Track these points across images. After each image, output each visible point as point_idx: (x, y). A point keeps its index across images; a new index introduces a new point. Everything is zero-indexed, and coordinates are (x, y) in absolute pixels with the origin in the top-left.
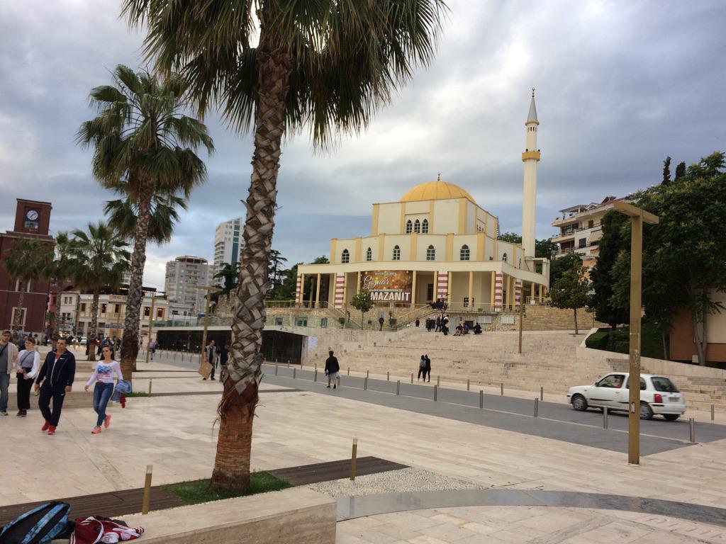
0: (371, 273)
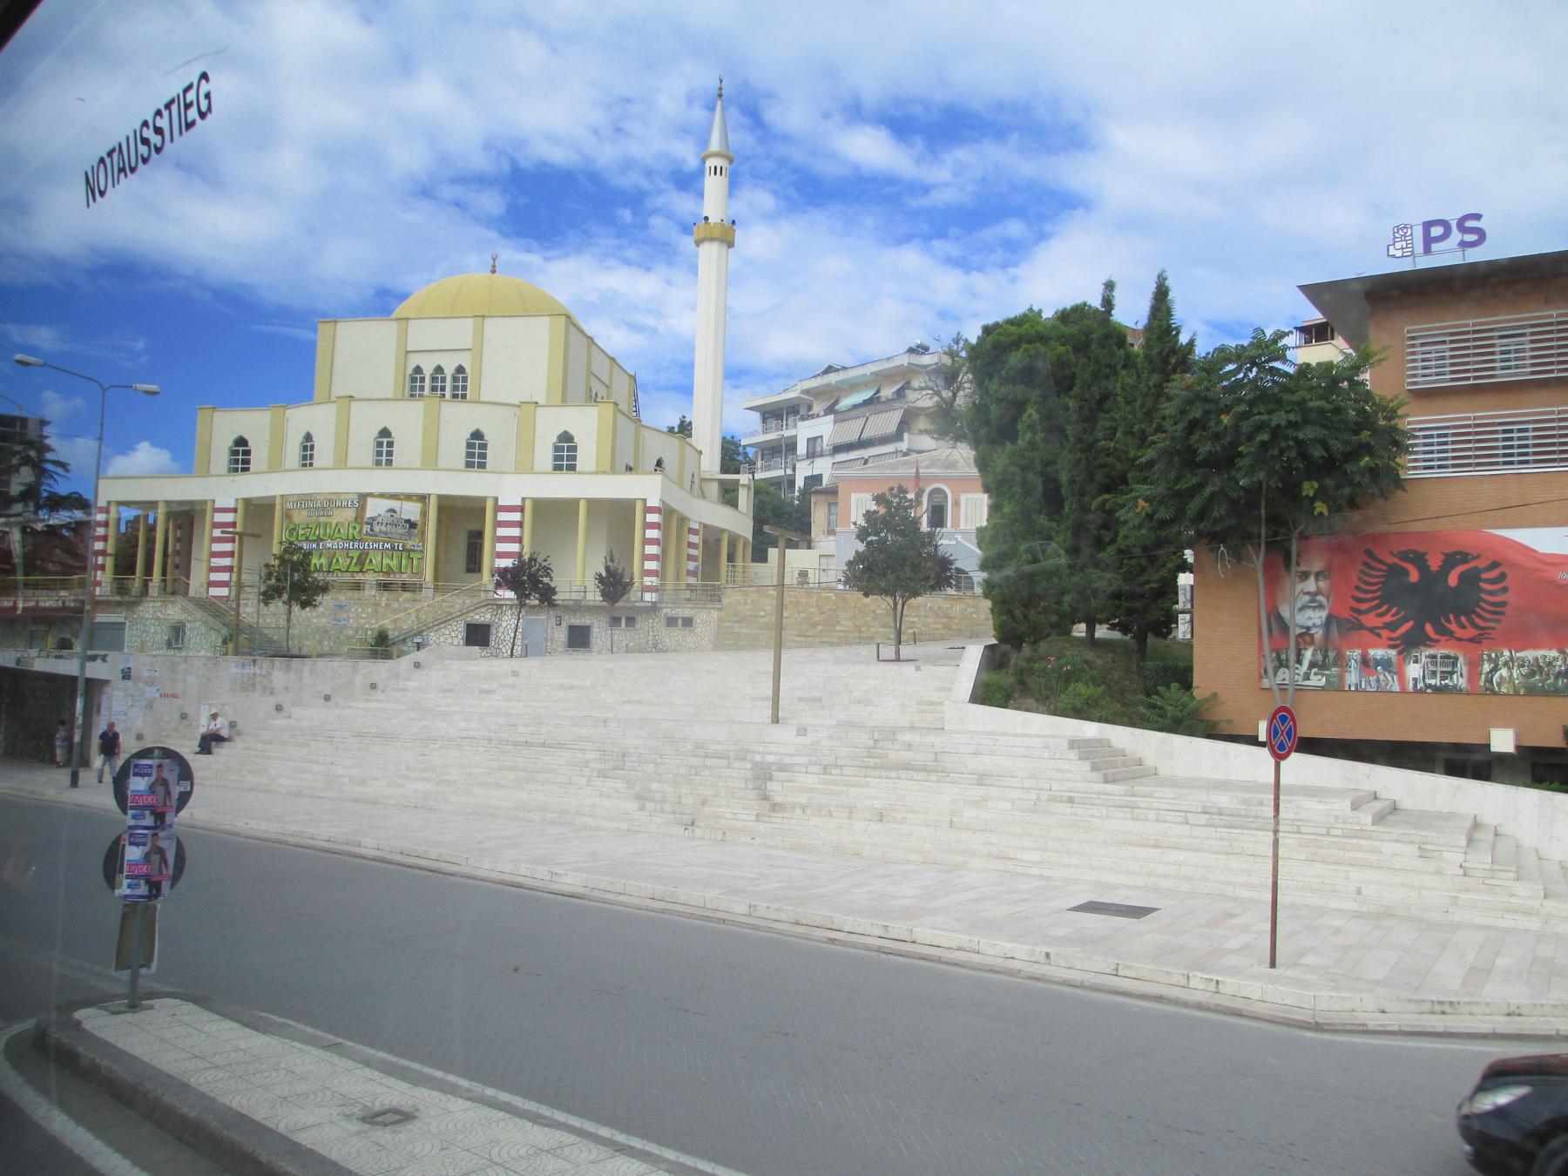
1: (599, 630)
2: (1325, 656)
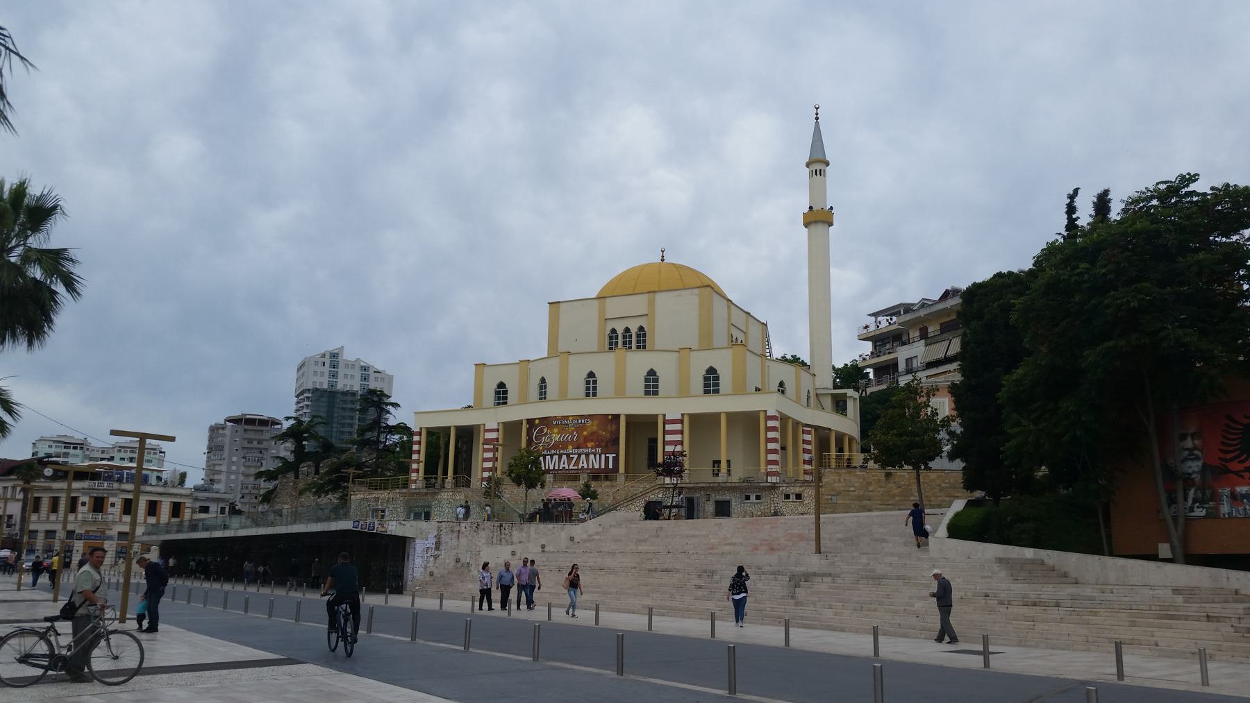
0: (546, 421)
1: (736, 506)
2: (1204, 494)
